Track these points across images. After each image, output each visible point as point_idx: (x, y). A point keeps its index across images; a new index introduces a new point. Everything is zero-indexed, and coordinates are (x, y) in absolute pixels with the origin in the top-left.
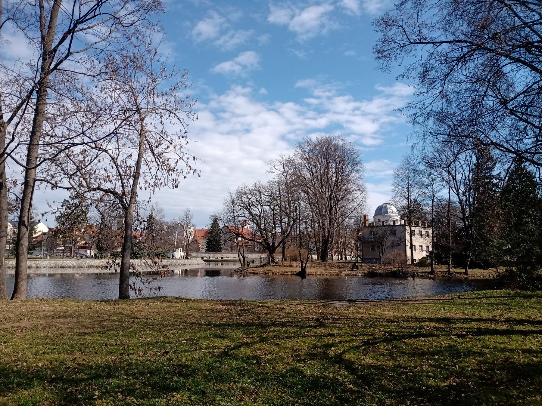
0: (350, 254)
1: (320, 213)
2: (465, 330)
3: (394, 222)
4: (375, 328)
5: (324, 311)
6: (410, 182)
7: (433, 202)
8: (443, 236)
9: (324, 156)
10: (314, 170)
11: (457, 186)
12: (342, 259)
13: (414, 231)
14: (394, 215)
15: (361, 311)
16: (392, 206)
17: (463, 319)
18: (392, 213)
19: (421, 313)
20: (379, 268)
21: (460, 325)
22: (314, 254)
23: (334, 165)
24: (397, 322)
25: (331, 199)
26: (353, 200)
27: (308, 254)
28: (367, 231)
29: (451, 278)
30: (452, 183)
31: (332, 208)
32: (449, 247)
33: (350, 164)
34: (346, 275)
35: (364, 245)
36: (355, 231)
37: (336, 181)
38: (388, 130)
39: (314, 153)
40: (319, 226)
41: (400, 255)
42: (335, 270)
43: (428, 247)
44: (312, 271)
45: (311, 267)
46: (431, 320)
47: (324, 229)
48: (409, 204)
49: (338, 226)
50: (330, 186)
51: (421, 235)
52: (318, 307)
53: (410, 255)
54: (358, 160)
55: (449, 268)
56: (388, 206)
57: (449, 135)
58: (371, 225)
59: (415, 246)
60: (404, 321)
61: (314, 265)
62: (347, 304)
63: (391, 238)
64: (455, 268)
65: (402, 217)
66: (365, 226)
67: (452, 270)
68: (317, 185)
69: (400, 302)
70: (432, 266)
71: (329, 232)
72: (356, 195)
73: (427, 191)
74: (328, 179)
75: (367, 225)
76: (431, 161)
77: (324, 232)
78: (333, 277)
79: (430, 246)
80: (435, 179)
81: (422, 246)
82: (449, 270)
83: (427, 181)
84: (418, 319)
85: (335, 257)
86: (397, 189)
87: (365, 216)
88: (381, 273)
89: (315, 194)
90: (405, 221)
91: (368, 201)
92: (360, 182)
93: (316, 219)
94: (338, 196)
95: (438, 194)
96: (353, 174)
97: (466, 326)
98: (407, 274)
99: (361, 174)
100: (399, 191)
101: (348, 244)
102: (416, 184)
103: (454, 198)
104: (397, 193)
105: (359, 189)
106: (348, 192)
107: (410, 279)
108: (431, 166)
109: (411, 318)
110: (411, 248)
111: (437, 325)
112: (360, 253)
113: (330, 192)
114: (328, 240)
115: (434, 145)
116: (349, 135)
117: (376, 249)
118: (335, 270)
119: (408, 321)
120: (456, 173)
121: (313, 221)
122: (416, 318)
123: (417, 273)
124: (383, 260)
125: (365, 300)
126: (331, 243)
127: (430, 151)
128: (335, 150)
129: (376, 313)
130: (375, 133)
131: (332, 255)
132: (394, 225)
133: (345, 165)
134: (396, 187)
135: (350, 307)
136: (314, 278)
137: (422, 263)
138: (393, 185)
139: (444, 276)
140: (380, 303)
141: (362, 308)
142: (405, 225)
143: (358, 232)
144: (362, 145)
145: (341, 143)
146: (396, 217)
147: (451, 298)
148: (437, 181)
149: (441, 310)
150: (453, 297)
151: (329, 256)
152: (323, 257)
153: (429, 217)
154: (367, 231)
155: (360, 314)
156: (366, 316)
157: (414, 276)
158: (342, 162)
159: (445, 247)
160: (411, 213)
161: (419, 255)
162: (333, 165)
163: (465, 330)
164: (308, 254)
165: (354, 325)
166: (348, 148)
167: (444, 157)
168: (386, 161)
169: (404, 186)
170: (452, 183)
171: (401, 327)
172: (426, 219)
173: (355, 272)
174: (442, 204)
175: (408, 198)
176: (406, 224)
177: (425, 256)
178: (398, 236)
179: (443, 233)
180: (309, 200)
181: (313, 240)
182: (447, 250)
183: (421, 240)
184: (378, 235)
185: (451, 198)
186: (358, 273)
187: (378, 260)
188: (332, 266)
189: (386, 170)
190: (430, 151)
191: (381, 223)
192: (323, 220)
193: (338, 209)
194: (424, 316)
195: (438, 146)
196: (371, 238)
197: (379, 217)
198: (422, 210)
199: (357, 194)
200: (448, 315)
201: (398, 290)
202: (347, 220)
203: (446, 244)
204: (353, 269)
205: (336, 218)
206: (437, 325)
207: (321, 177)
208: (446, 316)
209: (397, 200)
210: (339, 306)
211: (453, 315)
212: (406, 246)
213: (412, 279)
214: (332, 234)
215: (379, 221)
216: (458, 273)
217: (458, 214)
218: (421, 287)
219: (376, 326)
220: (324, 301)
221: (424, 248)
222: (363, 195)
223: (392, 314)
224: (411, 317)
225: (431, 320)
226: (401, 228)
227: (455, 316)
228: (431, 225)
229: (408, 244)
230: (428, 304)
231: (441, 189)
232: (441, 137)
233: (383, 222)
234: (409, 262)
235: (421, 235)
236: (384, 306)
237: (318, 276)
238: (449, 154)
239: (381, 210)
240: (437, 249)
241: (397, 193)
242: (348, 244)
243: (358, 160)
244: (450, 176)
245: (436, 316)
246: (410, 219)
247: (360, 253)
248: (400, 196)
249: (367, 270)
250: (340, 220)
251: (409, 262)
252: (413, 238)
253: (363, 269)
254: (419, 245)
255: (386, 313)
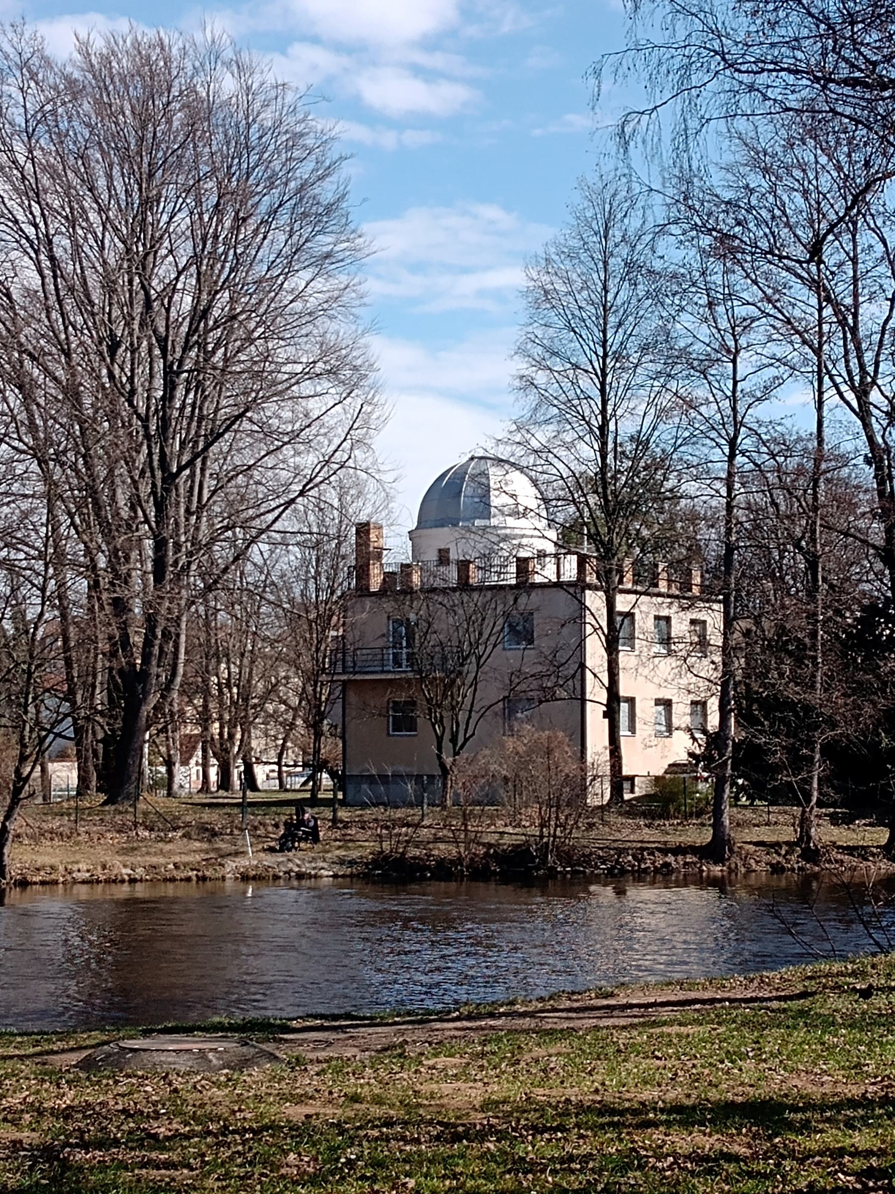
0: (273, 756)
1: (98, 506)
2: (858, 1164)
3: (523, 564)
4: (374, 1179)
5: (91, 1095)
6: (615, 339)
7: (732, 457)
8: (781, 644)
9: (126, 158)
10: (62, 245)
11: (862, 366)
12: (225, 782)
13: (630, 615)
14: (526, 528)
15: (306, 1083)
16: (516, 475)
17: (852, 1103)
18: (515, 514)
19: (635, 1080)
20: (431, 834)
21: (832, 1137)
22: (62, 756)
23: (183, 221)
24: (502, 1136)
25: (165, 423)
26: (294, 436)
27: (23, 759)
28: (371, 622)
29: (816, 876)
30: (835, 349)
31: (170, 479)
32: (808, 709)
33: (283, 218)
34: (245, 878)
35: (352, 698)
36: (309, 619)
37: (200, 314)
38: (506, 28)
39: (62, 136)
40: (94, 586)
41: (549, 752)
42: (181, 853)
43: (699, 706)
44: (41, 860)
45: (37, 837)
46: (685, 1115)
47: (120, 606)
48: (604, 466)
49: (209, 588)
50: (163, 342)
51: (666, 640)
52: (55, 1076)
53: (607, 755)
54: (326, 191)
55: (804, 823)
56: (495, 474)
57: (825, 81)
58: (397, 585)
59: (631, 701)
60: (537, 1130)
61: (55, 824)
62: (229, 1046)
63: (506, 658)
64: (835, 820)
65: (568, 538)
66: (363, 590)
67: (825, 833)
68: (81, 340)
69: (527, 1022)
70: (718, 813)
71: (150, 621)
72: (315, 407)
73: (701, 392)
74: (148, 304)
75: (375, 584)
76: (726, 223)
77: (124, 628)
78: (170, 890)
79: (713, 704)
80: (748, 323)
81: (667, 704)
82: (805, 837)
83: (704, 332)
84: (613, 1112)
85: (188, 776)
86: (541, 378)
87: (363, 529)
88: (441, 862)
89: (72, 394)
90: (582, 560)
91: (378, 441)
92: (337, 329)
93: (74, 548)
94: (209, 408)
95: (761, 412)
96: (298, 280)
97: (861, 1140)
98: (586, 859)
99: (343, 279)
100: (554, 389)
101: (265, 697)
102: (644, 349)
103: (846, 435)
104: (544, 400)
105: (332, 372)
106: (267, 384)
107: (605, 894)
108: (726, 247)
109: (581, 1108)
110: (611, 714)
111: (707, 1141)
112: (330, 748)
113: (159, 382)
114: (144, 676)
115: (741, 124)
116: (281, 43)
117: (422, 722)
118: (181, 853)
119: (561, 1128)
120: (856, 295)
121: (57, 559)
122: (605, 1109)
123: (639, 853)
124: (457, 785)
125: (339, 1021)
126: (167, 688)
127: (719, 161)
128: (191, 125)
129: (393, 1094)
130: (430, 43)
131: (169, 763)
132: (524, 584)
133: (252, 223)
134: (540, 365)
135: (244, 1063)
136: (52, 904)
137: (667, 797)
138: (521, 351)
139: (777, 869)
140: (420, 1034)
141: (313, 1069)
142: (580, 585)
143: (324, 621)
144: (358, 110)
145: (228, 85)
146: (535, 535)
147: (799, 988)
148: (758, 333)
149: (744, 1057)
150: (812, 986)
151: (151, 768)
152: (114, 774)
153: (711, 538)
154: (371, 622)
155: (301, 1099)
156: (332, 1113)
157: (622, 873)
158: (235, 200)
159: (790, 705)
160: (617, 519)
161: (650, 756)
162: (177, 220)
163: (858, 1164)
164: (23, 759)
165: (258, 1170)
166: (268, 118)
167: (798, 198)
168: (491, 212)
169: (583, 361)
170: (835, 349)
171: (521, 1165)
172: (695, 550)
173: (298, 860)
174: (778, 468)
175: (603, 428)
176: (592, 579)
177: (683, 758)
178: (544, 644)
179: (781, 630)
180: (32, 428)
181: (54, 674)
182: (800, 721)
183: (667, 666)
184: (433, 639)
185: (827, 432)
186: (319, 862)
187: (432, 784)
188: (164, 825)
189: (488, 268)
190: (719, 161)
191: (452, 574)
192: (114, 553)
193: (210, 483)
194: (648, 1094)
195: (769, 134)
196: (397, 662)
197: (443, 537)
198: (675, 497)
199: (319, 399)
200: (777, 1083)
201: (532, 949)
202: (259, 552)
203: (793, 692)
204: (285, 844)
205: (194, 541)
206: (707, 1141)
207: (109, 287)
208: (762, 1092)
209: (541, 436)
210: (183, 1063)
211: (801, 1084)
212: (583, 701)
213: (609, 891)
214: (166, 635)
215: (443, 558)
216: (850, 850)
217: (862, 524)
218: (660, 928)
219: (379, 1164)
220: (98, 1036)
221: (682, 715)
222: (353, 403)
223: (475, 1093)
224: (580, 1105)
225: (685, 1115)
226: (562, 602)
227: (810, 1089)
228: (724, 583)
229: (596, 692)
230: (676, 1029)
231: (778, 382)
232: (776, 84)
233: (463, 566)
234: (600, 793)
235: (666, 640)
236: (438, 1048)
237: (83, 891)
238: (825, 182)
239: (455, 497)
240: (746, 719)
241: (544, 400)
242: (265, 697)
243: (326, 191)
244: (828, 311)
245: (713, 1095)
246: (607, 552)
247: (330, 748)
248: (562, 419)
249: (365, 847)
250: (222, 552)
251: (600, 793)
252: (625, 659)
253: (346, 841)
254: (655, 699)
255: (447, 1088)
